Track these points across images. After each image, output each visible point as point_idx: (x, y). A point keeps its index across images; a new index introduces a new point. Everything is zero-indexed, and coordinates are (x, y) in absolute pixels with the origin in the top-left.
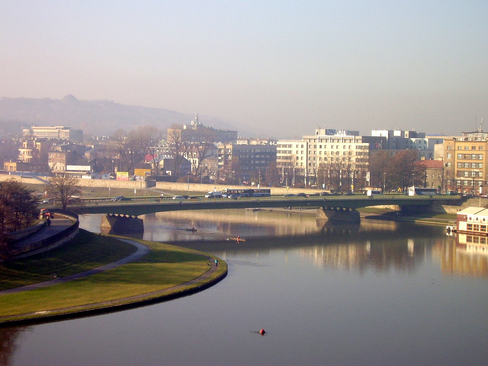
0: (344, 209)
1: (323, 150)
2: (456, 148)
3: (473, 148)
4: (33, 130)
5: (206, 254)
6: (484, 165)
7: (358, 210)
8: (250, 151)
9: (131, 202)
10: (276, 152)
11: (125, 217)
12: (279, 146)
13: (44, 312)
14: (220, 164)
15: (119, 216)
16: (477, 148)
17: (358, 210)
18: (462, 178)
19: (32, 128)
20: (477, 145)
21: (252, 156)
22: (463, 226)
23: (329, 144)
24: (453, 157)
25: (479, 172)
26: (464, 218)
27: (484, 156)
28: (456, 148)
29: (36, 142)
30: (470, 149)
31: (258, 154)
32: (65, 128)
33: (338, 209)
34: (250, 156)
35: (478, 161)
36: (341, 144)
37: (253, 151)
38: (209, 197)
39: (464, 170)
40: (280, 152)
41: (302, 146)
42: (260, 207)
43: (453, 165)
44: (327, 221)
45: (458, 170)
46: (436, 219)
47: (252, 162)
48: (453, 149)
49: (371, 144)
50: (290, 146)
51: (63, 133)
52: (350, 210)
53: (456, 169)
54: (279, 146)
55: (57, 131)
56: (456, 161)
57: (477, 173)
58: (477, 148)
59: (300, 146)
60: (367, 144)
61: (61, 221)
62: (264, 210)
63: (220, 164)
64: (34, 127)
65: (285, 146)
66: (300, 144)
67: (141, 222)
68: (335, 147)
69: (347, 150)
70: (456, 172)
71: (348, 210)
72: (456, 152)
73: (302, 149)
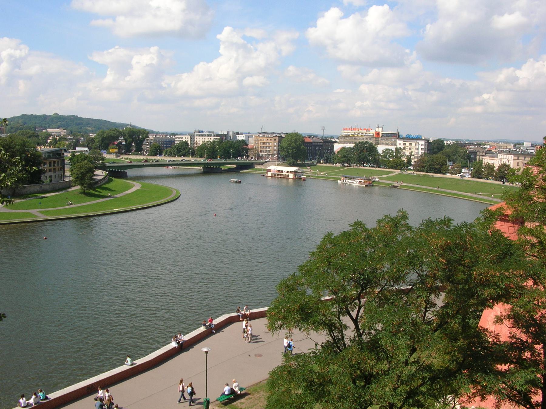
3: (268, 140)
6: (272, 147)
7: (221, 167)
10: (174, 141)
11: (112, 170)
12: (177, 138)
13: (117, 209)
14: (147, 146)
15: (115, 170)
16: (269, 140)
17: (221, 167)
18: (262, 153)
20: (269, 139)
21: (163, 146)
22: (269, 174)
23: (201, 137)
24: (258, 144)
26: (269, 171)
29: (56, 136)
30: (266, 140)
31: (166, 141)
32: (64, 130)
33: (206, 166)
34: (162, 143)
35: (269, 146)
36: (207, 138)
37: (163, 140)
40: (177, 141)
42: (55, 195)
43: (258, 148)
47: (163, 146)
48: (258, 140)
52: (218, 167)
53: (260, 149)
54: (177, 138)
55: (60, 131)
56: (260, 145)
57: (269, 151)
58: (269, 140)
59: (187, 138)
61: (181, 166)
62: (247, 173)
63: (147, 146)
64: (48, 129)
65: (180, 138)
66: (187, 137)
68: (204, 139)
69: (203, 140)
70: (260, 151)
71: (216, 167)
72: (260, 142)
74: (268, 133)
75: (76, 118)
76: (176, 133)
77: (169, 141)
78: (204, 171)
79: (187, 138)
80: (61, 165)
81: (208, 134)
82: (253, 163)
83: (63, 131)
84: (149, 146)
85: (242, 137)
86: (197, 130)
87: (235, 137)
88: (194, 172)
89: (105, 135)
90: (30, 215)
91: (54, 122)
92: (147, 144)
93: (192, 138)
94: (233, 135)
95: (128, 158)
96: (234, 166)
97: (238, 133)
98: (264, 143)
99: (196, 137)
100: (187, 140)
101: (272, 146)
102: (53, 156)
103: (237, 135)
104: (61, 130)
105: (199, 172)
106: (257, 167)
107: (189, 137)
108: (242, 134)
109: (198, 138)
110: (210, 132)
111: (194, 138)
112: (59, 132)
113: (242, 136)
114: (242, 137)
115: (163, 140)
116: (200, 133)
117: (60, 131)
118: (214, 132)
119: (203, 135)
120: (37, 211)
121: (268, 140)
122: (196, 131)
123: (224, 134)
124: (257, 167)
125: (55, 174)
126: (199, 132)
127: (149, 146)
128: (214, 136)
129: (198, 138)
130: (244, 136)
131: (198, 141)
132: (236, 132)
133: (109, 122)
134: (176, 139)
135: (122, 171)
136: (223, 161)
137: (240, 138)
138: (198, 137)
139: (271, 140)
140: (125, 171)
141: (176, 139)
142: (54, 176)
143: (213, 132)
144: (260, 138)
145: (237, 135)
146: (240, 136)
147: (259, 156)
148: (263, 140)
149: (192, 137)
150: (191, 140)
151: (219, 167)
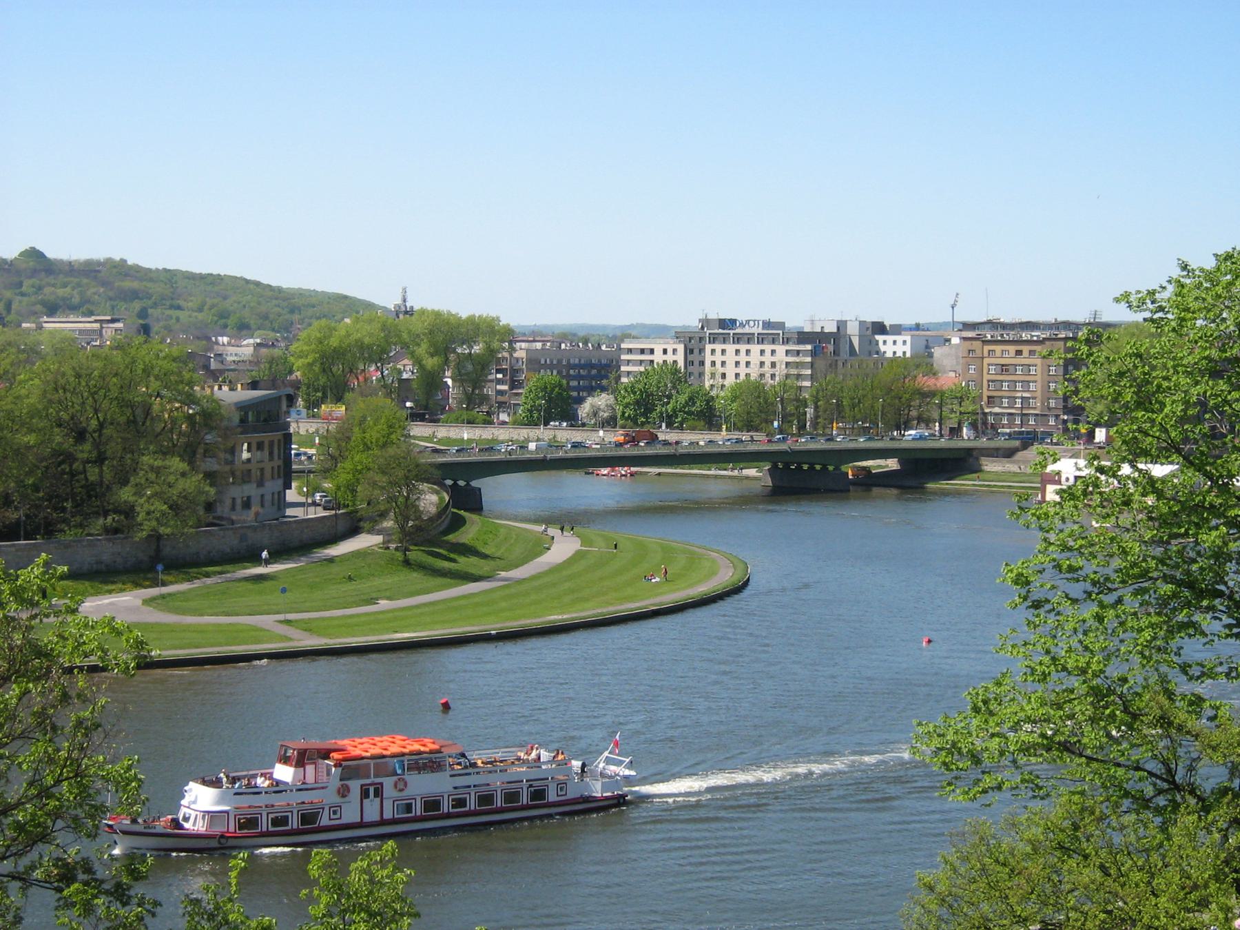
0: (818, 467)
1: (743, 358)
2: (986, 354)
3: (1019, 353)
4: (45, 325)
5: (452, 556)
6: (1039, 385)
8: (559, 361)
9: (445, 457)
14: (499, 387)
16: (1026, 353)
18: (997, 410)
19: (41, 320)
20: (1026, 349)
23: (731, 348)
25: (1029, 398)
27: (1039, 368)
28: (986, 354)
30: (1012, 354)
31: (574, 367)
32: (113, 321)
37: (564, 363)
38: (706, 445)
39: (999, 394)
41: (904, 342)
44: (770, 488)
45: (991, 394)
46: (959, 482)
48: (978, 353)
49: (815, 347)
50: (652, 351)
51: (109, 331)
52: (831, 468)
53: (986, 393)
55: (97, 326)
56: (986, 377)
58: (1026, 353)
60: (809, 347)
63: (499, 387)
64: (45, 319)
65: (642, 351)
67: (478, 493)
70: (985, 399)
71: (824, 468)
72: (986, 361)
73: (713, 358)
74: (1005, 326)
75: (121, 269)
76: (619, 334)
77: (590, 366)
78: (774, 486)
79: (670, 351)
80: (279, 458)
81: (760, 331)
82: (969, 451)
83: (111, 325)
84: (505, 387)
85: (900, 342)
86: (713, 316)
87: (870, 346)
88: (716, 490)
89: (334, 342)
90: (257, 633)
91: (24, 289)
92: (500, 376)
93: (692, 351)
94: (860, 336)
95: (434, 436)
96: (892, 464)
97: (880, 328)
98: (1004, 369)
99: (709, 347)
100: (670, 358)
101: (1038, 378)
102: (1063, 419)
103: (877, 337)
104: (101, 321)
105: (757, 487)
106: (991, 466)
107: (681, 348)
108: (897, 330)
109: (718, 352)
110: (767, 324)
111: (702, 351)
112: (94, 331)
113: (899, 339)
114: (900, 342)
115: (564, 363)
116: (725, 330)
117: (97, 326)
118: (784, 323)
119: (738, 339)
120: (281, 622)
121: (1019, 353)
122: (705, 323)
123: (822, 333)
124: (991, 466)
125: (261, 491)
126: (723, 323)
127: (505, 387)
128: (786, 341)
129: (718, 352)
130: (908, 339)
131: (718, 365)
132: (873, 323)
133: (258, 284)
134: (623, 357)
135: (462, 483)
136: (862, 442)
137: (894, 347)
138: (718, 347)
139: (1032, 353)
140: (474, 484)
141: (623, 357)
142: (259, 499)
143: (781, 325)
144: (987, 348)
145: (880, 338)
146: (890, 338)
147: (195, 423)
148: (998, 354)
149: (693, 343)
150: (690, 358)
151: (837, 468)
